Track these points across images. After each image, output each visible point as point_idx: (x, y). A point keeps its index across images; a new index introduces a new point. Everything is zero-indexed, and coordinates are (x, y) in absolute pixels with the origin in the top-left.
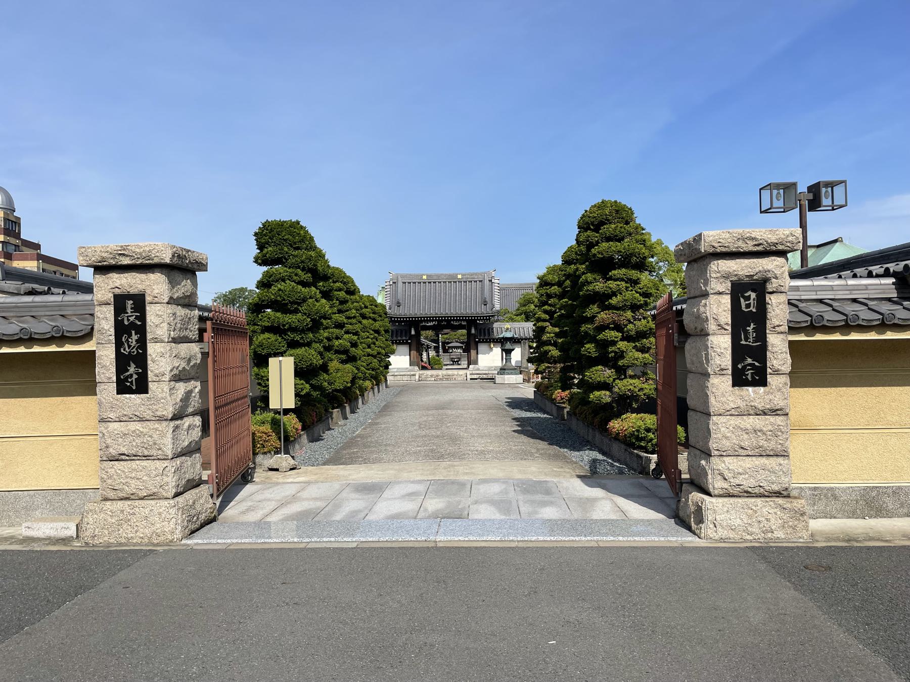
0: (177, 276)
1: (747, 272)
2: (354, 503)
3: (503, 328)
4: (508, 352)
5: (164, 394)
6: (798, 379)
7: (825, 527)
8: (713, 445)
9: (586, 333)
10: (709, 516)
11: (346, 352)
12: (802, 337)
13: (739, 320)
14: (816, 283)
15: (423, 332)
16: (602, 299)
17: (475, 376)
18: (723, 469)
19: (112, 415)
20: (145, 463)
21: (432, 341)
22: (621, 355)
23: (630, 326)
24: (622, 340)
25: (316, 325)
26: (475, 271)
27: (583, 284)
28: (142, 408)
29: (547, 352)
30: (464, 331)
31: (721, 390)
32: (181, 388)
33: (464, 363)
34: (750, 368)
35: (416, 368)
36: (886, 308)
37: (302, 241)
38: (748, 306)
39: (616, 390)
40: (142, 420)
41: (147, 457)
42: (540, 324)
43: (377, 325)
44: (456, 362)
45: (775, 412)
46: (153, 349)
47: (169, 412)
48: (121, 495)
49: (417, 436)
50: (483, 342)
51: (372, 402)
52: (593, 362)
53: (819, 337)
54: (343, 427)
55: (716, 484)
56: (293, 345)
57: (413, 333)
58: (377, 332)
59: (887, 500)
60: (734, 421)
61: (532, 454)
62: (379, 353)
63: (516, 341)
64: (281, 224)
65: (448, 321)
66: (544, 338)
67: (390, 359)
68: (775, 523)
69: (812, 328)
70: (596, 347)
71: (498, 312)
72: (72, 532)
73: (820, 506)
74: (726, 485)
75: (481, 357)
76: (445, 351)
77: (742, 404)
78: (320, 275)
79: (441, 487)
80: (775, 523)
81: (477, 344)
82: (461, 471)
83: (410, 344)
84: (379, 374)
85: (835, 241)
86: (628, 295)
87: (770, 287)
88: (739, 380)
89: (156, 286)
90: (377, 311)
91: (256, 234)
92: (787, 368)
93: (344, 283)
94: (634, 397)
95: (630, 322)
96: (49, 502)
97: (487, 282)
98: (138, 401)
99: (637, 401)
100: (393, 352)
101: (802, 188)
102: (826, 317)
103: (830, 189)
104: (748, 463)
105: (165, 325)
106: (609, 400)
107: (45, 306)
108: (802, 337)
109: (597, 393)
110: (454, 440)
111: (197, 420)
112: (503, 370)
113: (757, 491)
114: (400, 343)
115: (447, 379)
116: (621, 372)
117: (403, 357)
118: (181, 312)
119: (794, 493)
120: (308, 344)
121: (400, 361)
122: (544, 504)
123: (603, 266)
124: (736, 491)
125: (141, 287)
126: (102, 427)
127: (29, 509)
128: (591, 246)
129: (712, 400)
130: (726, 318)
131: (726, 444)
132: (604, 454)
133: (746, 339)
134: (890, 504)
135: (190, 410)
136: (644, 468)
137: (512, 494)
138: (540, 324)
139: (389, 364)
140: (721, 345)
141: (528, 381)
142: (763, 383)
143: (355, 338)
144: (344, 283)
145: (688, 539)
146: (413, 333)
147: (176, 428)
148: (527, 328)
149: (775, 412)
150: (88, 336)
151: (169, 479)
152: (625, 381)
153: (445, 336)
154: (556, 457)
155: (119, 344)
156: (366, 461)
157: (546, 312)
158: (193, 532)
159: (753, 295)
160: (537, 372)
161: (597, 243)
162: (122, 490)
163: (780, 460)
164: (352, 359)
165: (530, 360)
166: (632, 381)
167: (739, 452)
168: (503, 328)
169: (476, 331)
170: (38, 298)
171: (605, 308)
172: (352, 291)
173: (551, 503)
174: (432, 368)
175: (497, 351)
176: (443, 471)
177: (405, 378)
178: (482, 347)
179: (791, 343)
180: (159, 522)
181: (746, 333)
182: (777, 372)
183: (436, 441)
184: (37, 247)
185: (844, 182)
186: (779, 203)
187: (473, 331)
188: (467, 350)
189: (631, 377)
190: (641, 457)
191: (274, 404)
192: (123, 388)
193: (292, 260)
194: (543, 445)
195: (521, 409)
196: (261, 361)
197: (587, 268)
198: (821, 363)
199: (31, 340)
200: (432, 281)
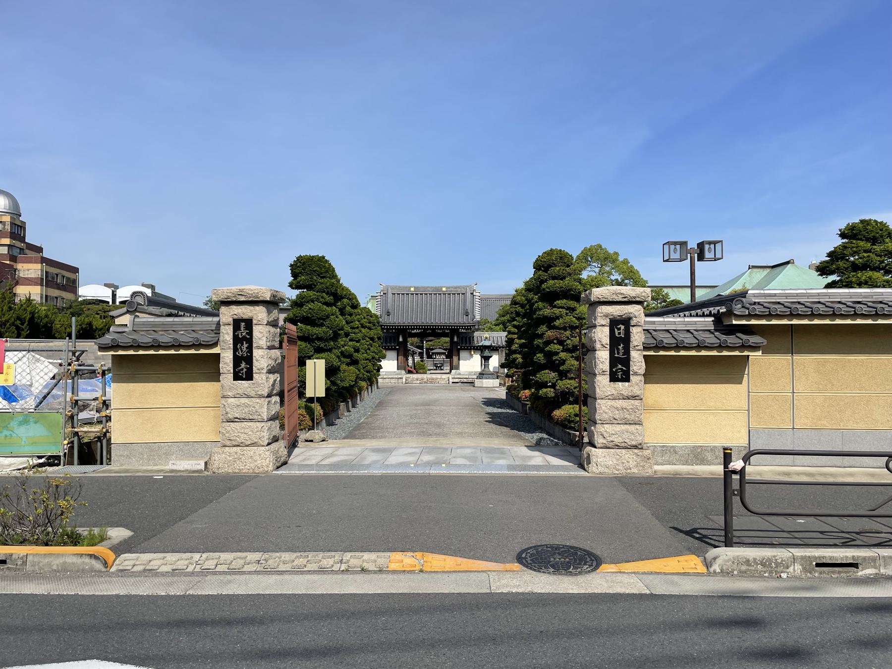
0: (271, 307)
1: (619, 313)
2: (373, 457)
3: (483, 337)
4: (486, 359)
5: (263, 381)
6: (649, 377)
7: (663, 469)
8: (597, 417)
9: (538, 346)
10: (593, 459)
11: (350, 356)
12: (652, 353)
13: (615, 342)
14: (666, 320)
15: (409, 339)
16: (549, 321)
17: (457, 380)
18: (603, 432)
19: (230, 394)
20: (250, 424)
21: (418, 347)
22: (563, 362)
23: (569, 342)
24: (562, 351)
25: (336, 336)
26: (458, 285)
27: (536, 310)
28: (249, 390)
29: (515, 360)
30: (448, 339)
31: (603, 384)
32: (272, 377)
33: (447, 368)
34: (620, 371)
35: (403, 372)
36: (702, 336)
37: (327, 272)
38: (619, 334)
39: (558, 387)
40: (249, 397)
41: (251, 420)
42: (510, 336)
43: (372, 333)
44: (439, 367)
45: (634, 397)
46: (256, 353)
47: (265, 392)
48: (234, 443)
49: (410, 423)
50: (464, 349)
51: (368, 399)
52: (542, 367)
53: (662, 353)
54: (349, 417)
55: (599, 441)
56: (319, 350)
57: (401, 339)
58: (372, 339)
59: (707, 454)
60: (610, 403)
61: (496, 435)
62: (373, 358)
63: (494, 349)
64: (311, 259)
65: (433, 330)
66: (513, 348)
67: (381, 363)
68: (632, 464)
69: (657, 348)
70: (544, 356)
71: (479, 322)
72: (202, 467)
73: (666, 457)
74: (605, 441)
77: (614, 392)
78: (340, 297)
79: (431, 450)
80: (632, 464)
82: (444, 442)
83: (398, 350)
84: (372, 377)
85: (788, 263)
86: (568, 319)
87: (633, 323)
88: (614, 378)
89: (259, 314)
90: (372, 321)
91: (291, 266)
92: (642, 371)
93: (350, 299)
94: (571, 393)
95: (568, 338)
96: (182, 450)
97: (469, 295)
98: (247, 385)
99: (573, 396)
100: (384, 357)
101: (693, 245)
102: (665, 341)
103: (712, 246)
104: (618, 428)
105: (264, 338)
106: (553, 395)
107: (182, 324)
108: (652, 353)
109: (545, 390)
110: (439, 425)
111: (278, 399)
112: (481, 375)
113: (623, 445)
114: (389, 349)
115: (431, 382)
116: (563, 375)
118: (272, 330)
119: (645, 446)
120: (330, 350)
121: (389, 365)
122: (499, 458)
123: (550, 297)
124: (611, 445)
125: (250, 315)
126: (223, 401)
127: (168, 454)
128: (542, 282)
129: (598, 390)
130: (606, 340)
131: (606, 416)
132: (550, 435)
133: (618, 353)
134: (709, 456)
135: (275, 392)
136: (572, 441)
137: (478, 454)
138: (510, 336)
139: (380, 367)
140: (603, 357)
141: (504, 385)
142: (627, 380)
143: (358, 344)
144: (350, 299)
145: (582, 473)
146: (401, 339)
147: (269, 402)
148: (500, 337)
149: (634, 397)
150: (215, 344)
151: (265, 434)
152: (564, 381)
153: (430, 343)
154: (514, 436)
155: (235, 350)
156: (373, 438)
157: (514, 326)
158: (278, 468)
159: (623, 327)
160: (507, 376)
161: (546, 281)
162: (235, 440)
163: (637, 426)
164: (354, 362)
165: (33, 313)
166: (569, 381)
167: (613, 421)
168: (483, 337)
169: (458, 340)
170: (176, 319)
171: (551, 327)
172: (355, 306)
173: (503, 458)
174: (417, 373)
175: (477, 357)
176: (431, 442)
177: (393, 381)
178: (463, 354)
179: (645, 356)
180: (261, 460)
181: (618, 349)
182: (636, 374)
183: (425, 426)
184: (39, 250)
185: (721, 241)
186: (677, 256)
187: (456, 339)
188: (449, 356)
189: (570, 379)
190: (569, 434)
191: (309, 393)
192: (237, 377)
193: (319, 287)
194: (505, 430)
195: (494, 406)
196: (302, 363)
197: (539, 298)
198: (661, 368)
199: (159, 347)
200: (419, 292)
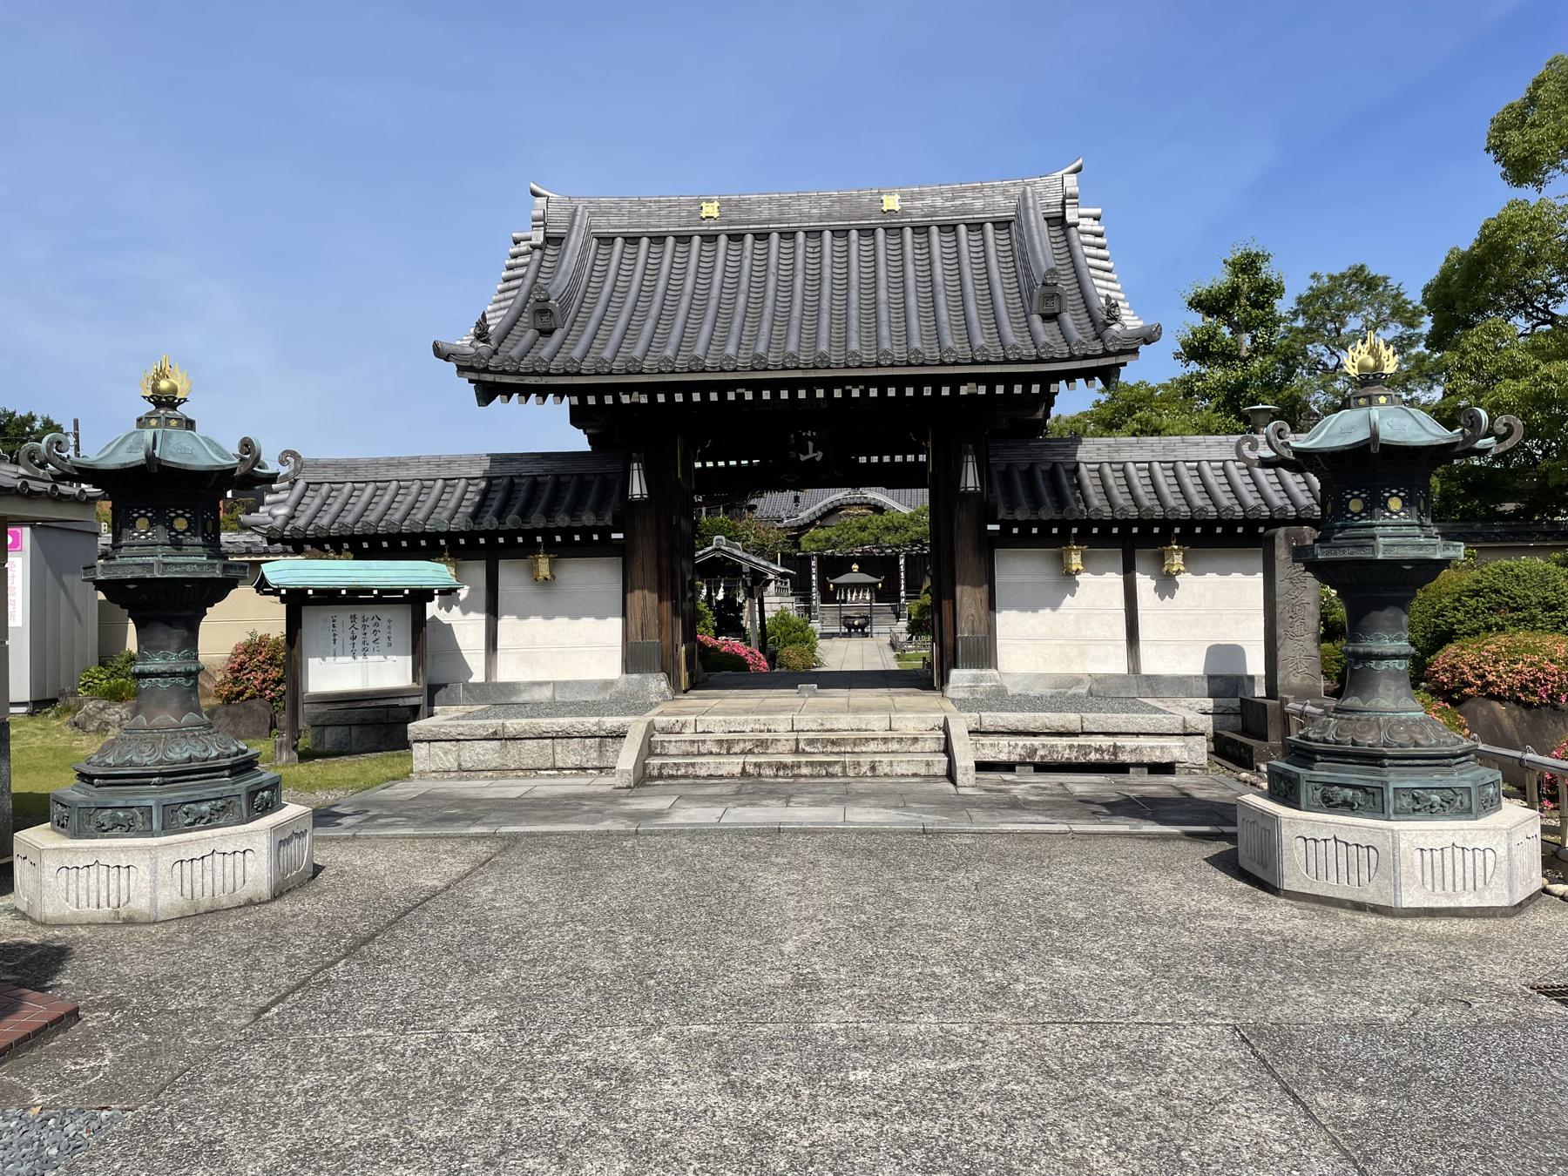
12: (1227, 829)
17: (1003, 750)
50: (1025, 541)
75: (1008, 622)
76: (827, 597)
81: (987, 548)
117: (588, 623)
178: (1014, 570)
179: (1235, 824)
187: (971, 480)
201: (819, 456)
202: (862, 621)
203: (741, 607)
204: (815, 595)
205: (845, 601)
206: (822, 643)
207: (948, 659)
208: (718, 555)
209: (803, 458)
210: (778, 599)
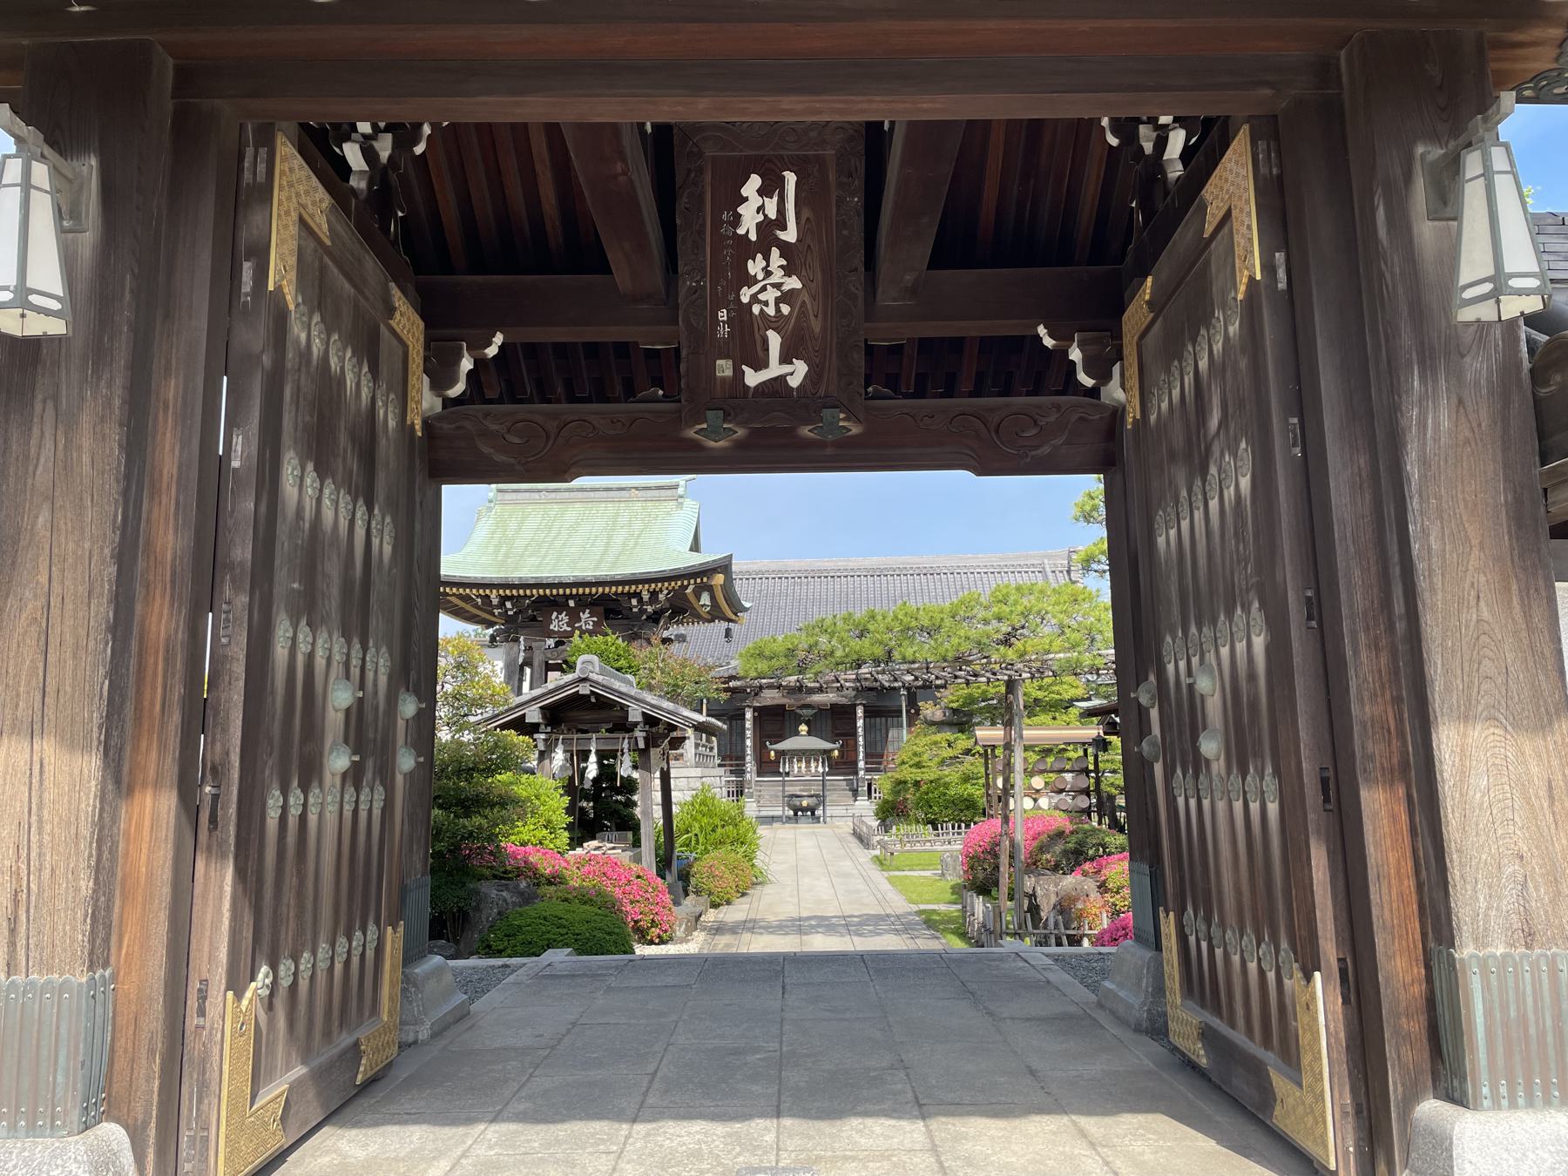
201: (798, 372)
202: (812, 801)
203: (629, 786)
204: (750, 765)
205: (788, 774)
206: (763, 831)
207: (1403, 1053)
208: (584, 689)
209: (752, 378)
210: (698, 772)
